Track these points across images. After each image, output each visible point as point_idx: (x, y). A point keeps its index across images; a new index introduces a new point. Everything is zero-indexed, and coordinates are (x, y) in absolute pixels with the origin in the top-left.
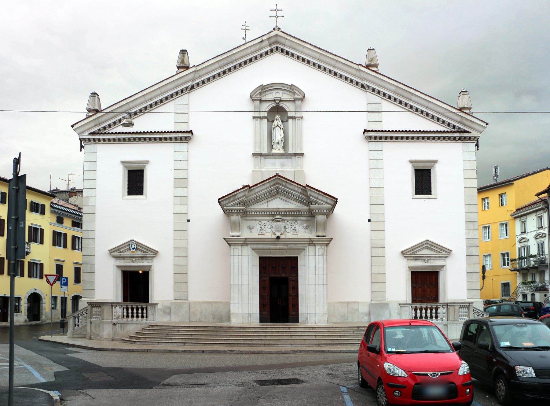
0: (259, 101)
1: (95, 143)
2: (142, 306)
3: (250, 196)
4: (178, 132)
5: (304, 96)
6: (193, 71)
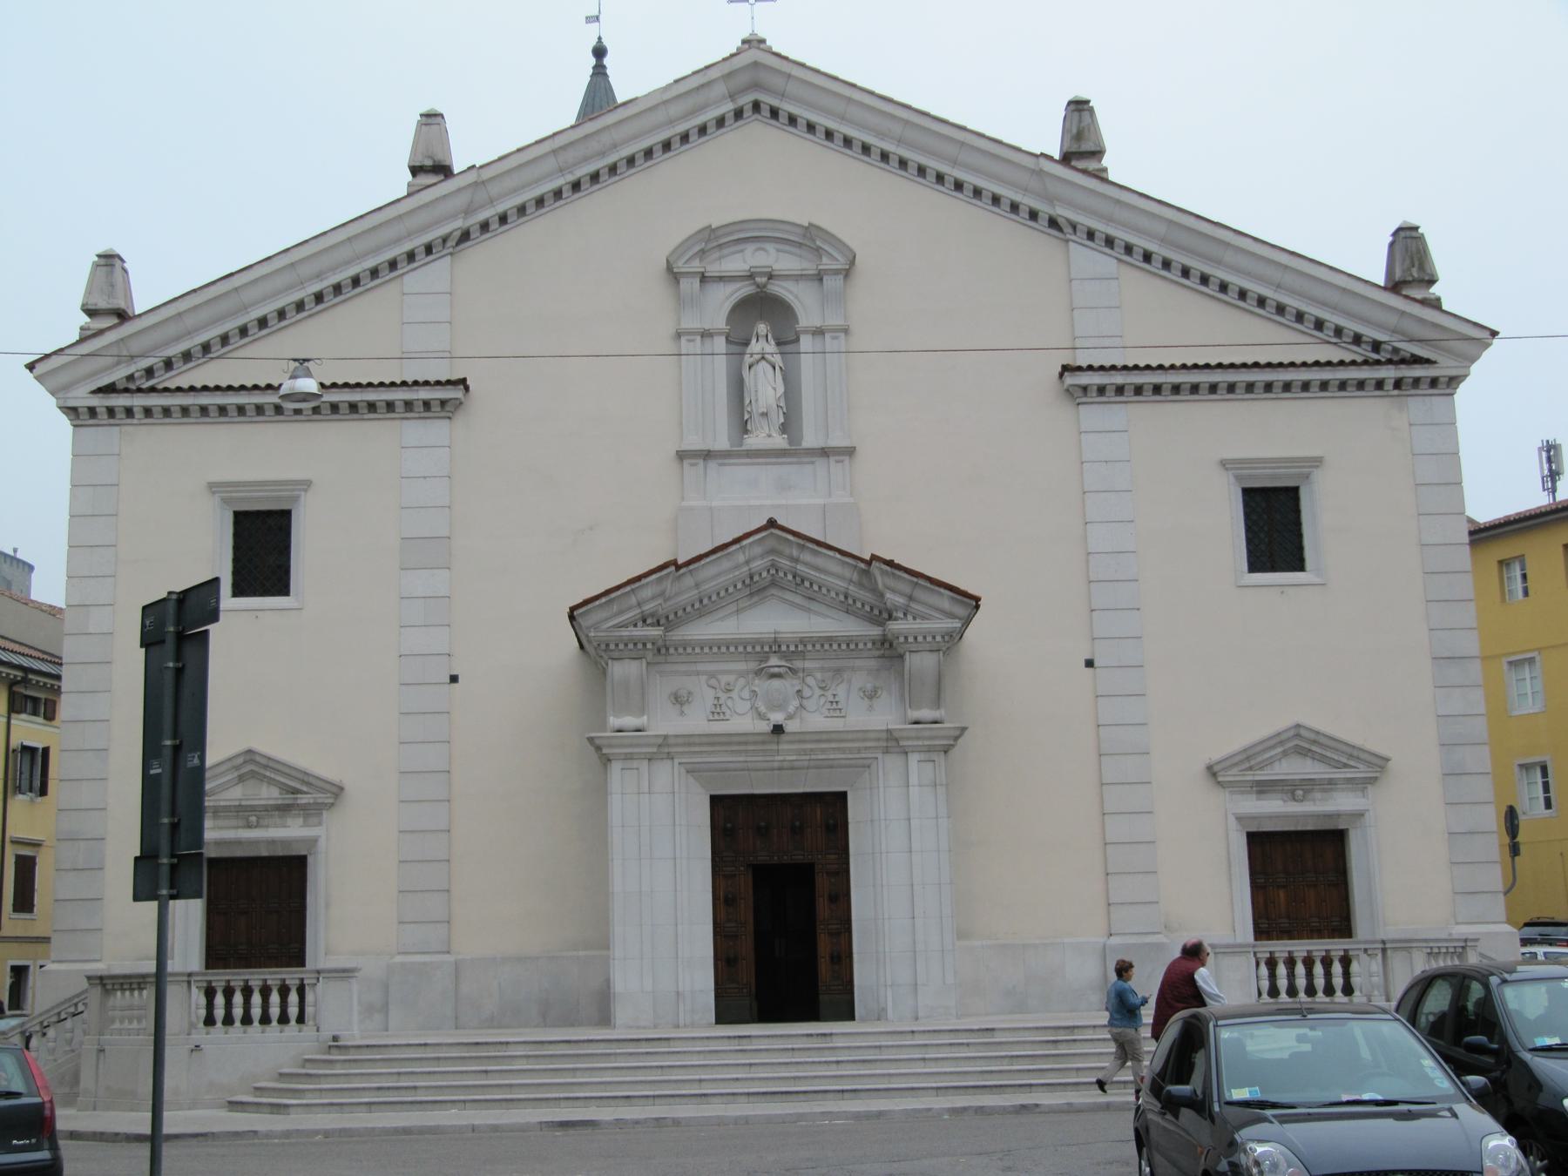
0: (841, 277)
1: (112, 421)
2: (284, 980)
3: (677, 594)
4: (416, 383)
5: (852, 262)
6: (469, 185)
